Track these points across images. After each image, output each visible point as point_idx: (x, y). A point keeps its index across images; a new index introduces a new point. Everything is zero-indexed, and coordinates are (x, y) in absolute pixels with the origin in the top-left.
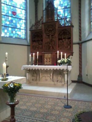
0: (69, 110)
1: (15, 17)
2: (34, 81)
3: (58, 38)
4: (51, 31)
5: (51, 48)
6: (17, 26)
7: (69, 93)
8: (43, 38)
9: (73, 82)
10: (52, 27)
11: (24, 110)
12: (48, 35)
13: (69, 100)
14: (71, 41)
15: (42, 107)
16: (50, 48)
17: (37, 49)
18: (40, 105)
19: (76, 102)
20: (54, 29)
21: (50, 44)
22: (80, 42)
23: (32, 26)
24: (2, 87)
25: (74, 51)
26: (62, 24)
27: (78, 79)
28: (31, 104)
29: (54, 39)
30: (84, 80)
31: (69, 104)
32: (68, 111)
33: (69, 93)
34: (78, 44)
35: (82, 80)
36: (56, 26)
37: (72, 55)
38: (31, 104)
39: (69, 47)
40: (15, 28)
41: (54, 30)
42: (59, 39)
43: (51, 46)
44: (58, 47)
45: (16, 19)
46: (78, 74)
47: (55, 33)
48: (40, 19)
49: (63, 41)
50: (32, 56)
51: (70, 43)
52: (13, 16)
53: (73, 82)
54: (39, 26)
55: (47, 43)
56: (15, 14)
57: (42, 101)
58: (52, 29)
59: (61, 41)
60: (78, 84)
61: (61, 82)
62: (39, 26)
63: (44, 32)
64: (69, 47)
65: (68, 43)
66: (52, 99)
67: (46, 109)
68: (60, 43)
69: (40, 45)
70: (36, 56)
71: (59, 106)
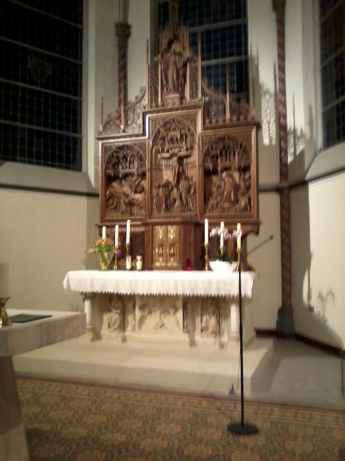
0: (249, 441)
2: (112, 329)
7: (248, 373)
9: (261, 333)
11: (79, 445)
13: (248, 401)
15: (148, 431)
18: (140, 424)
19: (277, 411)
22: (285, 184)
25: (262, 217)
26: (276, 409)
27: (278, 323)
28: (105, 419)
30: (301, 328)
31: (250, 417)
32: (246, 447)
33: (248, 373)
34: (278, 190)
35: (293, 324)
37: (257, 233)
38: (105, 419)
46: (277, 302)
48: (137, 98)
50: (110, 236)
53: (261, 333)
57: (145, 407)
64: (243, 202)
66: (185, 399)
67: (103, 451)
70: (123, 236)
71: (211, 426)
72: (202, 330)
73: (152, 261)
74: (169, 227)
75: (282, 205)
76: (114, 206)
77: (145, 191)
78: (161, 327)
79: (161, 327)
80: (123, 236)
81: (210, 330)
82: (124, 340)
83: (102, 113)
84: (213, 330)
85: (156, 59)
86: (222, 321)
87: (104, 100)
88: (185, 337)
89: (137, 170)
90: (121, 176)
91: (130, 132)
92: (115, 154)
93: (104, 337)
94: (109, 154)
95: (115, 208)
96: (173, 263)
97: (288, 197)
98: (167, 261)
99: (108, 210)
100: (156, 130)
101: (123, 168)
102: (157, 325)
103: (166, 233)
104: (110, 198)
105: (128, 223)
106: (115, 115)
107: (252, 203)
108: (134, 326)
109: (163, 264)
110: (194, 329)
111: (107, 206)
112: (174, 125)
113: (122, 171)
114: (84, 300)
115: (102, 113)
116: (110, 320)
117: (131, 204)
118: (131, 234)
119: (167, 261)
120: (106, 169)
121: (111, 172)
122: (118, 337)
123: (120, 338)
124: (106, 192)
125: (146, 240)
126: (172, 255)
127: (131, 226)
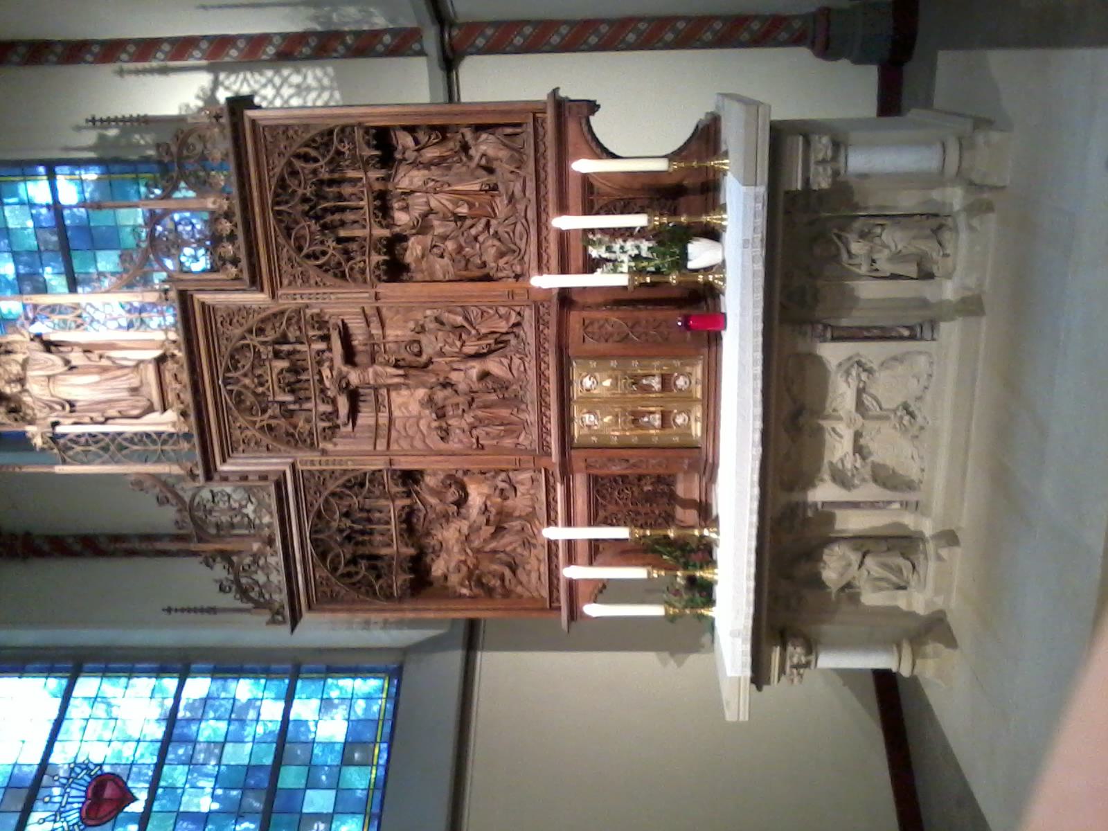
1: (142, 796)
3: (385, 289)
4: (295, 370)
5: (494, 366)
6: (250, 769)
8: (378, 464)
10: (246, 362)
12: (343, 404)
14: (411, 130)
16: (503, 385)
17: (508, 542)
20: (271, 336)
21: (446, 384)
22: (430, 40)
23: (244, 593)
24: (198, 97)
27: (861, 59)
29: (397, 332)
34: (449, 63)
36: (244, 310)
39: (486, 146)
40: (272, 790)
41: (284, 340)
42: (396, 270)
43: (475, 368)
44: (487, 278)
45: (175, 774)
47: (320, 322)
49: (423, 226)
50: (602, 591)
51: (442, 132)
52: (137, 807)
54: (239, 511)
55: (441, 415)
56: (109, 792)
58: (277, 355)
59: (414, 250)
60: (906, 91)
61: (937, 231)
62: (239, 511)
63: (308, 460)
65: (439, 162)
68: (441, 266)
69: (462, 502)
70: (596, 550)
72: (926, 275)
73: (691, 447)
74: (576, 392)
75: (496, 47)
76: (507, 573)
77: (460, 475)
78: (912, 415)
79: (912, 415)
80: (596, 550)
81: (927, 246)
82: (949, 538)
83: (212, 610)
84: (927, 237)
85: (38, 441)
86: (895, 208)
87: (175, 604)
88: (950, 331)
89: (393, 498)
90: (412, 551)
91: (269, 519)
92: (342, 569)
93: (939, 602)
94: (341, 588)
95: (513, 568)
96: (689, 379)
97: (474, 28)
98: (686, 399)
99: (519, 589)
100: (266, 440)
101: (389, 545)
102: (904, 430)
103: (592, 403)
104: (480, 583)
105: (550, 533)
106: (220, 571)
107: (491, 121)
108: (905, 505)
109: (698, 412)
110: (924, 303)
111: (507, 593)
112: (247, 381)
113: (395, 548)
114: (251, 556)
115: (212, 610)
116: (884, 584)
117: (499, 522)
118: (593, 521)
119: (686, 399)
120: (389, 597)
121: (400, 580)
122: (939, 558)
123: (944, 552)
124: (461, 596)
125: (616, 469)
126: (666, 382)
127: (569, 522)
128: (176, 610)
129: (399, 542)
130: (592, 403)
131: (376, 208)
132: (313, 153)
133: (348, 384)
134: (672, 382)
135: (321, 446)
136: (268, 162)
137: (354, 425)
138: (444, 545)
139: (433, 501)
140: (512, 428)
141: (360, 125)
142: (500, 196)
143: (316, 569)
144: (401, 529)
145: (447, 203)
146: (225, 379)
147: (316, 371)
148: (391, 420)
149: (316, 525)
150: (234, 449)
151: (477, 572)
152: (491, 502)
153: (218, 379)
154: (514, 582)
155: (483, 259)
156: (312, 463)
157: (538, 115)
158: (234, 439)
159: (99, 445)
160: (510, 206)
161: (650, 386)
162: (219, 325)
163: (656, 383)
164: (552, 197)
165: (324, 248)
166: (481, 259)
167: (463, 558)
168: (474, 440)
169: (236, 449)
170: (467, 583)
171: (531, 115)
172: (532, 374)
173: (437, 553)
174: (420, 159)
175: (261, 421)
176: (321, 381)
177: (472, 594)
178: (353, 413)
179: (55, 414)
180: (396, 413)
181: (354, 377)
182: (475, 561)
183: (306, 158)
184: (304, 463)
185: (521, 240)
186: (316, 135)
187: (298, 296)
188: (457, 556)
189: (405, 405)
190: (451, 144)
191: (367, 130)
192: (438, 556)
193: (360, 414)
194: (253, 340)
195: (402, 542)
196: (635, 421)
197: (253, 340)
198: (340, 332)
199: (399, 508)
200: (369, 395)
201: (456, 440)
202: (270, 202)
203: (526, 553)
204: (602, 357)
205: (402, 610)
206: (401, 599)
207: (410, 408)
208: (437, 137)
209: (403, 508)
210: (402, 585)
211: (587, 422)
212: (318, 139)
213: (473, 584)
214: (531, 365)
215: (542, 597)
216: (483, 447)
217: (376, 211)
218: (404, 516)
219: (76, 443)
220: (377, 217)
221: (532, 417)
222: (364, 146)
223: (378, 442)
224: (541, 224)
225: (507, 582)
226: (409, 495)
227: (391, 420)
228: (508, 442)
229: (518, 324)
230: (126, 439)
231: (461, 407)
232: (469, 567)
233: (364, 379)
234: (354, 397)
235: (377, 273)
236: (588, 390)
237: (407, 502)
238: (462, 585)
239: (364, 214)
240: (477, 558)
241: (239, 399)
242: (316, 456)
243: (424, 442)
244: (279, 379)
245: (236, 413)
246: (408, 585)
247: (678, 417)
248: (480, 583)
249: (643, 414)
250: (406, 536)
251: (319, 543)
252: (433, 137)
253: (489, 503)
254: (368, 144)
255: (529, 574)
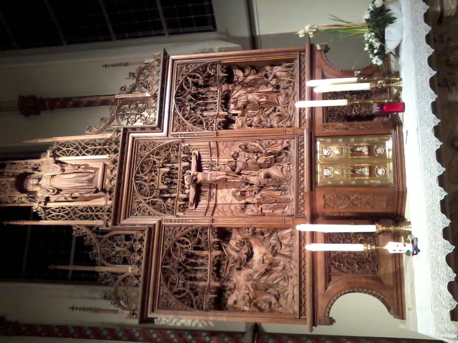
5: (274, 171)
12: (192, 192)
43: (262, 173)
69: (250, 255)
76: (274, 300)
100: (151, 209)
103: (330, 163)
111: (271, 311)
124: (243, 311)
128: (77, 309)
129: (211, 278)
130: (330, 163)
131: (222, 103)
132: (187, 240)
133: (196, 179)
134: (374, 151)
135: (177, 214)
136: (177, 78)
137: (196, 207)
138: (237, 286)
139: (233, 253)
140: (281, 203)
141: (219, 62)
142: (281, 95)
143: (162, 287)
144: (214, 271)
145: (256, 97)
146: (136, 177)
147: (181, 177)
148: (216, 205)
149: (166, 260)
150: (132, 214)
151: (255, 301)
152: (266, 257)
153: (132, 177)
154: (277, 305)
155: (271, 123)
156: (171, 221)
157: (302, 53)
158: (133, 208)
159: (64, 212)
160: (286, 98)
161: (361, 152)
162: (139, 151)
163: (365, 150)
164: (307, 69)
165: (185, 289)
166: (270, 123)
167: (247, 292)
168: (260, 209)
169: (133, 213)
170: (248, 304)
171: (298, 53)
172: (294, 173)
173: (232, 290)
174: (245, 80)
175: (149, 199)
176: (183, 182)
177: (251, 310)
178: (197, 200)
179: (49, 193)
180: (219, 202)
181: (200, 177)
182: (254, 294)
183: (182, 242)
184: (166, 220)
185: (291, 110)
186: (199, 67)
187: (179, 136)
188: (244, 292)
189: (224, 197)
190: (260, 74)
191: (223, 65)
192: (232, 293)
193: (200, 203)
194: (154, 158)
195: (212, 278)
196: (353, 171)
197: (154, 158)
198: (196, 157)
199: (214, 256)
200: (206, 191)
201: (250, 210)
202: (174, 94)
203: (286, 284)
204: (334, 137)
205: (207, 316)
206: (207, 310)
207: (227, 199)
208: (254, 72)
209: (216, 256)
210: (209, 302)
211: (325, 174)
212: (191, 233)
213: (252, 305)
214: (293, 167)
215: (294, 312)
216: (264, 215)
217: (222, 105)
218: (216, 262)
219: (55, 211)
220: (222, 107)
221: (292, 196)
222: (221, 73)
223: (207, 213)
224: (301, 82)
225: (273, 306)
226: (220, 249)
227: (216, 205)
228: (279, 212)
229: (286, 148)
230: (79, 210)
231: (254, 191)
232: (250, 297)
233: (205, 177)
234: (198, 187)
235: (219, 126)
236: (326, 156)
237: (218, 253)
238: (245, 305)
239: (217, 106)
240: (255, 293)
241: (140, 189)
242: (173, 218)
243: (232, 213)
244: (162, 178)
245: (137, 193)
246: (213, 301)
247: (379, 170)
248: (255, 305)
249: (358, 168)
250: (215, 275)
251: (166, 271)
252: (252, 72)
253: (265, 258)
254: (222, 72)
255: (286, 298)
